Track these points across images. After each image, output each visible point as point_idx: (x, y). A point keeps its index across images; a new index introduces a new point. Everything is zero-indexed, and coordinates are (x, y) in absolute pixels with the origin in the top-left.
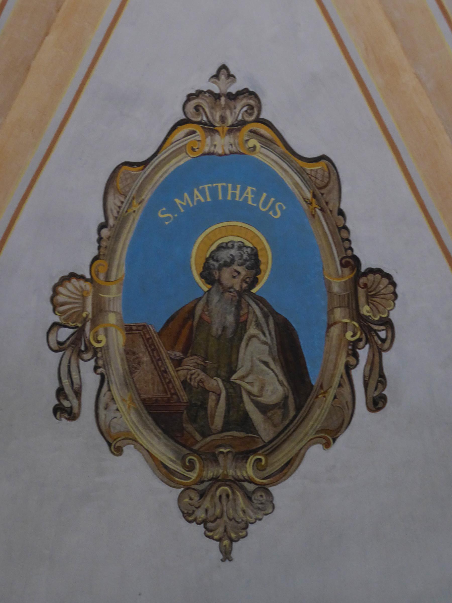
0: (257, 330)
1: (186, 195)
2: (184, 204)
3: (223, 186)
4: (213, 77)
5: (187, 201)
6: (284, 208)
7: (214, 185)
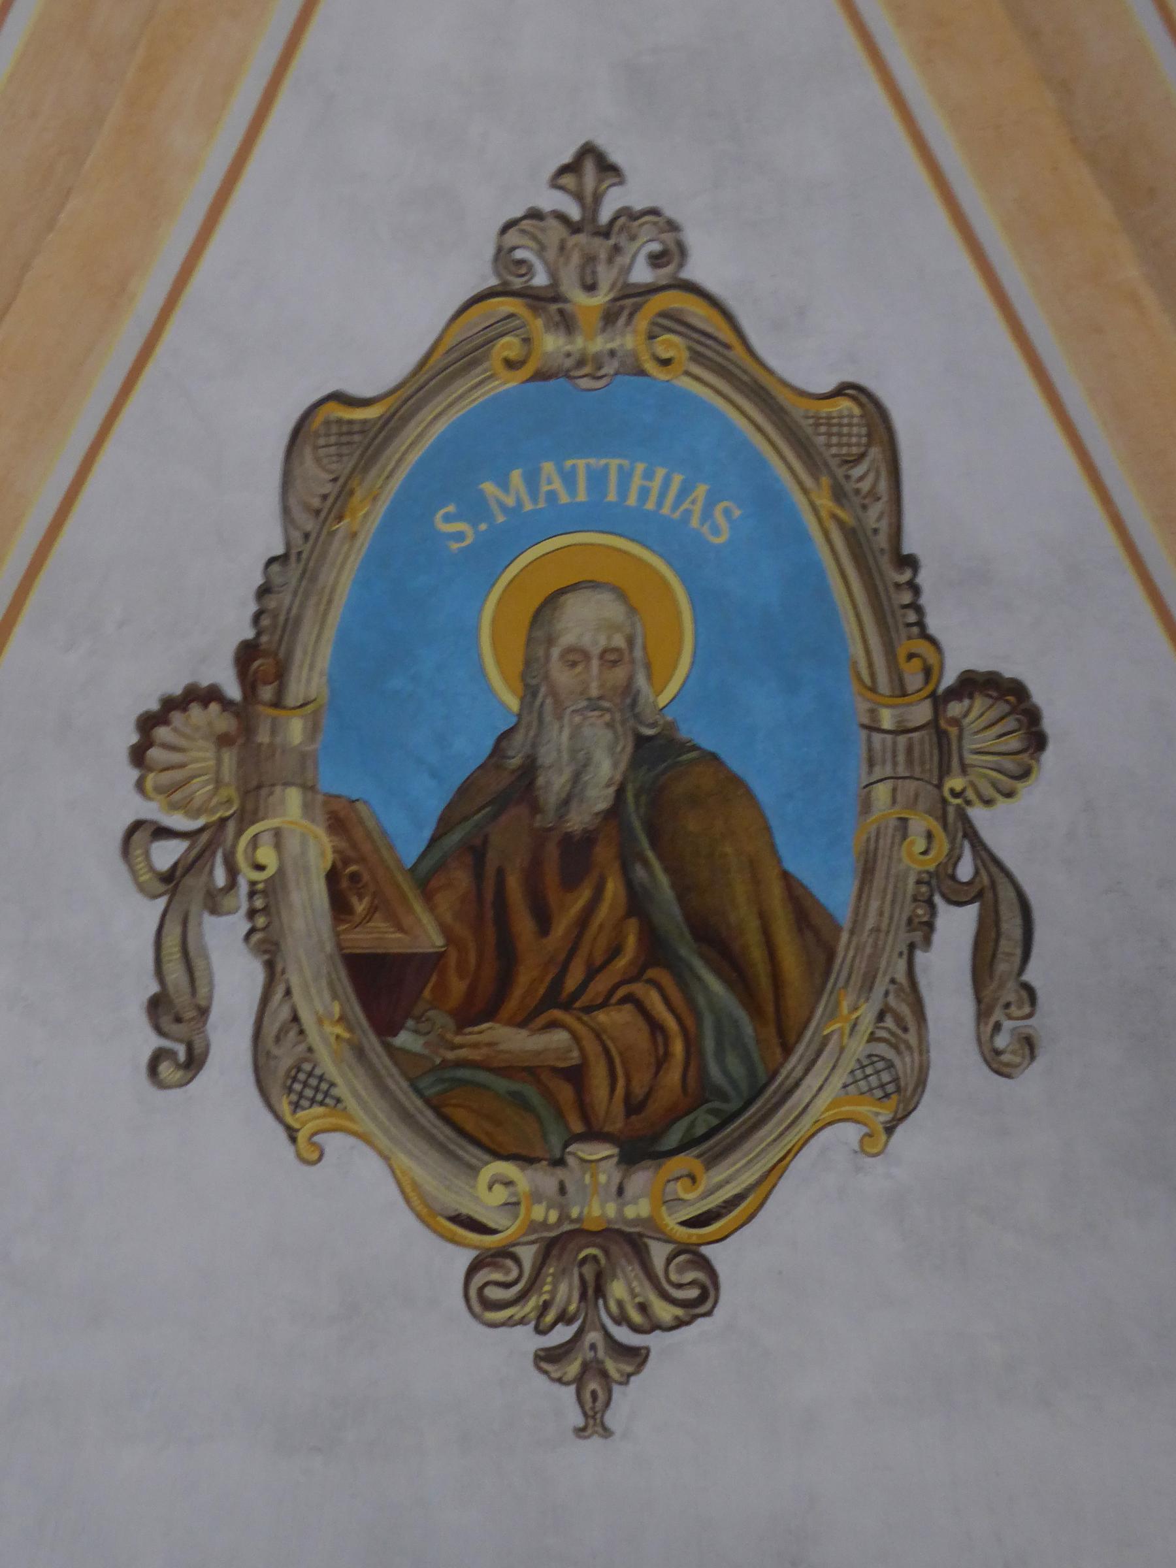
0: (891, 787)
1: (516, 477)
2: (510, 501)
3: (620, 467)
4: (564, 170)
5: (517, 493)
6: (455, 546)
7: (603, 462)
